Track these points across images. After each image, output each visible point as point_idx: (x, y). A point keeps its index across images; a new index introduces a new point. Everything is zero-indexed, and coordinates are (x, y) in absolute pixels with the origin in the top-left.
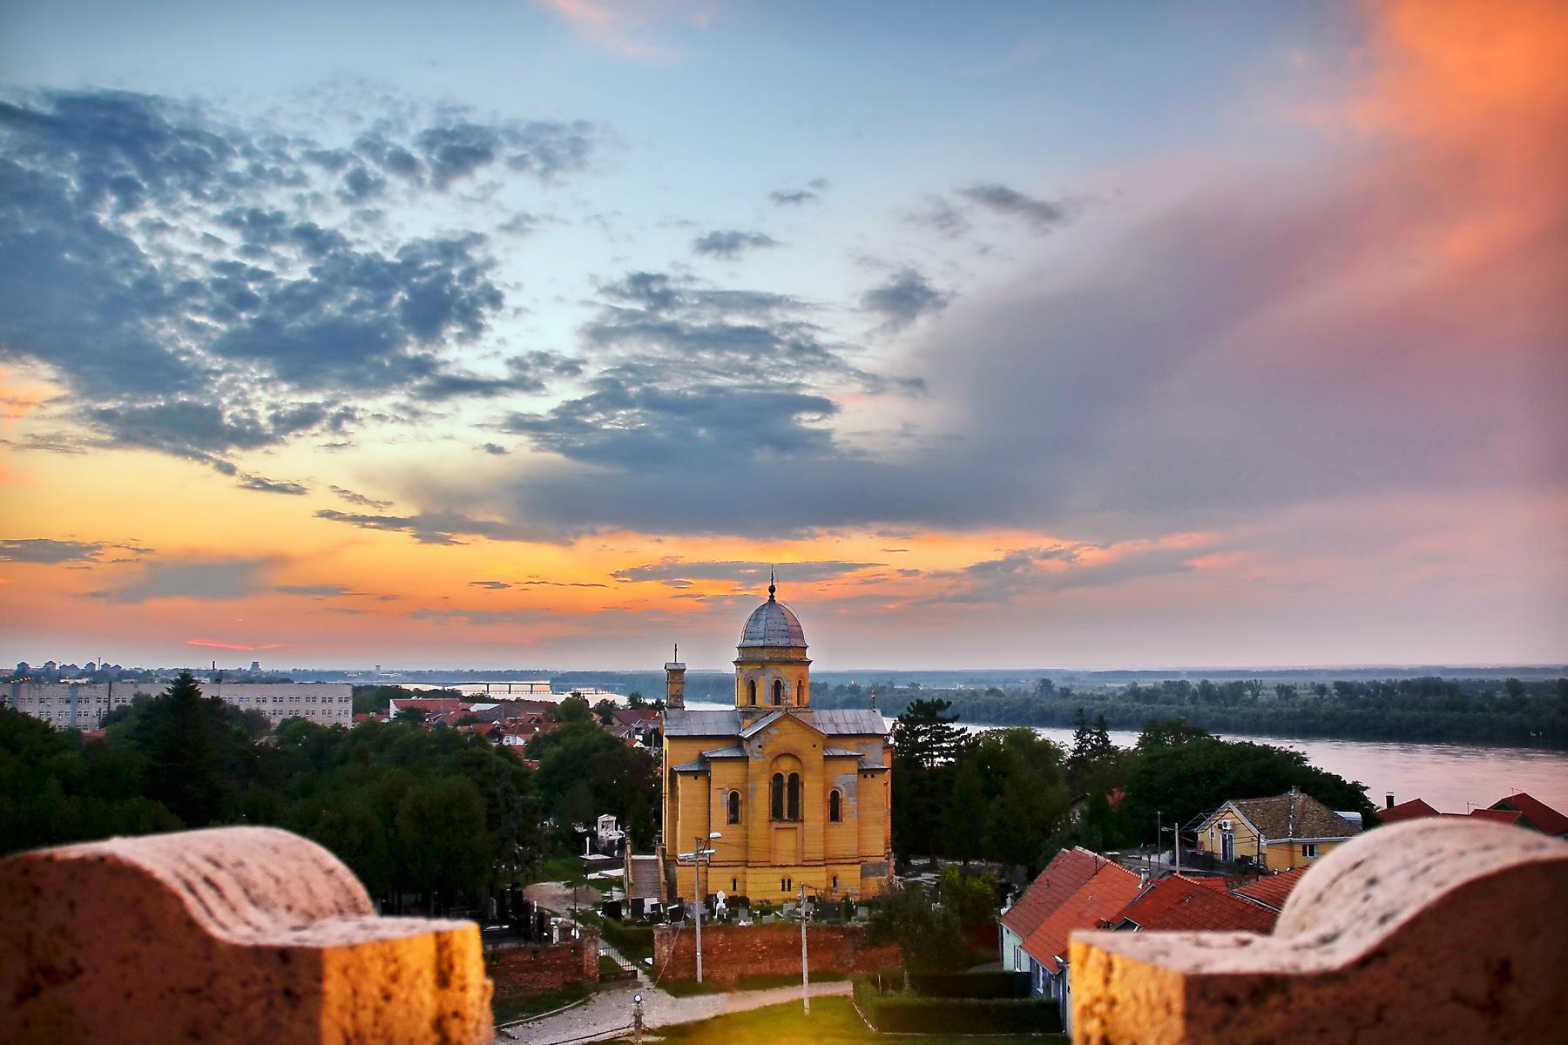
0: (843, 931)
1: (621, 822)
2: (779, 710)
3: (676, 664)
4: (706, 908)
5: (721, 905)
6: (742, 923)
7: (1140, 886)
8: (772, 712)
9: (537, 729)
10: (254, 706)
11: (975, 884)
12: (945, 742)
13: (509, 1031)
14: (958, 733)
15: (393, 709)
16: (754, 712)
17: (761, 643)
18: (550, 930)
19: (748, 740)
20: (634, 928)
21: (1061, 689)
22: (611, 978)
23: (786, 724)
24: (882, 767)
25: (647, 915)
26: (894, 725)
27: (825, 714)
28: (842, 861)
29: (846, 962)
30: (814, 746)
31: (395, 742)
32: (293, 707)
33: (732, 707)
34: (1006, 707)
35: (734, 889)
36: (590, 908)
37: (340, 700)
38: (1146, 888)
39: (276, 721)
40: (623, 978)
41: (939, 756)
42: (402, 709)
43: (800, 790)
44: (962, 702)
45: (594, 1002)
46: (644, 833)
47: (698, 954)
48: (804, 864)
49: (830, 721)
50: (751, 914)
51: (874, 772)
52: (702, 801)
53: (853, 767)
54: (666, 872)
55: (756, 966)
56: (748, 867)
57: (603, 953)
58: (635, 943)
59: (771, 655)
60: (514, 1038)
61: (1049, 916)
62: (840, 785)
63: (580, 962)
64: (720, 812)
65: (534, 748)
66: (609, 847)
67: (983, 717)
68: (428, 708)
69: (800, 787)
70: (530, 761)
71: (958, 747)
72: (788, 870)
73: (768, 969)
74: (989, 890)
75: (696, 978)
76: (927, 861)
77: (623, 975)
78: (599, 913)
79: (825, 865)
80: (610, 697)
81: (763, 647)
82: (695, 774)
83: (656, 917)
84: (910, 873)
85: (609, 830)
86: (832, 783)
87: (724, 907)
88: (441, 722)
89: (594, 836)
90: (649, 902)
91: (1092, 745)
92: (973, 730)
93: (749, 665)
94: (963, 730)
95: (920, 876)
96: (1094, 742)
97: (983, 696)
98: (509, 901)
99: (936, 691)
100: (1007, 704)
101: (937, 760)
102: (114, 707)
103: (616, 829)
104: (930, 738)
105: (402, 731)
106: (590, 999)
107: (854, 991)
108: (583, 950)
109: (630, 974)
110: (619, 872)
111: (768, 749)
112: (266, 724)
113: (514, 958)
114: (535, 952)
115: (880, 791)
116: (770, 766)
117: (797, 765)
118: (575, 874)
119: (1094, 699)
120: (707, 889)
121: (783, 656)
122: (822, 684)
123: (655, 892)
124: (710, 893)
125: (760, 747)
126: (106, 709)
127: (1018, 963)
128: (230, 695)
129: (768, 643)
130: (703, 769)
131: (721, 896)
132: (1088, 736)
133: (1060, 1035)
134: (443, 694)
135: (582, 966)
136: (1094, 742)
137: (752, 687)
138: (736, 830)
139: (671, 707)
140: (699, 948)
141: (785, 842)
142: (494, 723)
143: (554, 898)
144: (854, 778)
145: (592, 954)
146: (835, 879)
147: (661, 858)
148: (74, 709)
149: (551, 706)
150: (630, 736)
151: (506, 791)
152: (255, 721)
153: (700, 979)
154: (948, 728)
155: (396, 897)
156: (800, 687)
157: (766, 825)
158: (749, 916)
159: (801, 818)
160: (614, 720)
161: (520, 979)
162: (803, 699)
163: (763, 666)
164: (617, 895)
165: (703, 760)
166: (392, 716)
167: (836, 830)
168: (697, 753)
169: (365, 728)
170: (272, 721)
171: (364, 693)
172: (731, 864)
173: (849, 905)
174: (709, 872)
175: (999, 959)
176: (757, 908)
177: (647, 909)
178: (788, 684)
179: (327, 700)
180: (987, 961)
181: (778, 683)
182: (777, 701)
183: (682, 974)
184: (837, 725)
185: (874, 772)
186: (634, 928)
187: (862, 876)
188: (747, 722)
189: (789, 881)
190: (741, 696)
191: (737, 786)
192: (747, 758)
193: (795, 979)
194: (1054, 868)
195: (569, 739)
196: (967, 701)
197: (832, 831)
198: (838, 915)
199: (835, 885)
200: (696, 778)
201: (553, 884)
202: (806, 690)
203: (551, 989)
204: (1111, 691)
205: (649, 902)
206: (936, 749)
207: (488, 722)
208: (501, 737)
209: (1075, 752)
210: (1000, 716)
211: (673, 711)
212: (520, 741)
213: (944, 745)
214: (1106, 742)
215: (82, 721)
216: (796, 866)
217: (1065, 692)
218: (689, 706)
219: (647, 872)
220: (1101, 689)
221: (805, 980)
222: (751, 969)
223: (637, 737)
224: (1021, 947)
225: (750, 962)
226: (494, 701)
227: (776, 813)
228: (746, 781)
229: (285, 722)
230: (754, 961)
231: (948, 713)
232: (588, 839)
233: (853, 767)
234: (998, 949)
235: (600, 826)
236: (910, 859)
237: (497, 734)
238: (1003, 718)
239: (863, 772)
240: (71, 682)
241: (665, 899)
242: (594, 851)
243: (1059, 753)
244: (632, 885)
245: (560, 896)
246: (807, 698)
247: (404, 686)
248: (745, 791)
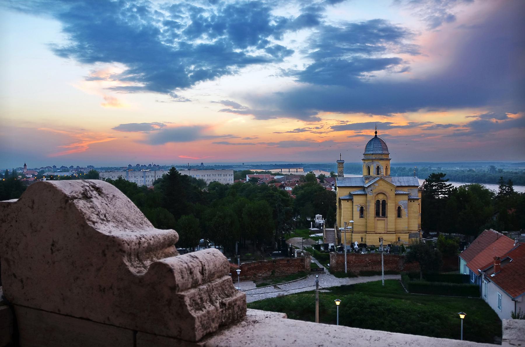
0: (399, 257)
1: (324, 217)
2: (378, 177)
3: (341, 160)
4: (351, 247)
5: (356, 246)
6: (363, 253)
7: (514, 245)
8: (376, 178)
9: (297, 184)
10: (201, 178)
11: (450, 242)
12: (443, 189)
13: (279, 286)
14: (448, 186)
15: (248, 178)
16: (369, 178)
17: (372, 153)
18: (294, 253)
19: (367, 188)
20: (324, 253)
21: (499, 169)
22: (315, 270)
23: (381, 182)
24: (417, 198)
25: (329, 249)
26: (424, 183)
27: (396, 178)
28: (402, 232)
29: (400, 268)
30: (392, 190)
31: (246, 189)
32: (214, 178)
33: (362, 176)
34: (476, 177)
35: (362, 241)
36: (310, 246)
37: (229, 175)
38: (517, 246)
39: (208, 183)
40: (319, 270)
41: (441, 194)
42: (250, 178)
43: (386, 206)
44: (458, 174)
45: (308, 278)
46: (331, 222)
47: (346, 263)
48: (388, 233)
49: (398, 181)
50: (367, 250)
51: (414, 200)
52: (350, 209)
53: (406, 198)
54: (338, 235)
55: (366, 268)
56: (367, 233)
57: (312, 261)
58: (324, 260)
59: (375, 157)
60: (280, 289)
61: (478, 254)
62: (401, 205)
63: (304, 264)
64: (357, 214)
65: (293, 192)
66: (320, 226)
67: (466, 180)
68: (260, 178)
69: (386, 205)
70: (294, 196)
71: (449, 191)
72: (382, 235)
73: (371, 269)
74: (456, 244)
75: (345, 271)
76: (436, 233)
77: (319, 269)
78: (313, 248)
79: (395, 233)
80: (323, 173)
81: (373, 154)
82: (347, 200)
83: (333, 250)
84: (429, 237)
85: (319, 220)
86: (398, 204)
87: (358, 247)
88: (263, 182)
89: (314, 222)
90: (331, 245)
91: (506, 191)
92: (456, 185)
93: (367, 160)
94: (450, 185)
95: (433, 238)
96: (507, 190)
97: (467, 172)
98: (281, 243)
99: (448, 170)
100: (476, 175)
101: (440, 196)
102: (157, 179)
103: (322, 220)
104: (438, 187)
105: (249, 185)
106: (307, 277)
107: (401, 278)
108: (305, 260)
109: (321, 269)
110: (321, 234)
111: (374, 191)
112: (205, 184)
113: (281, 262)
114: (288, 261)
115: (416, 207)
116: (375, 197)
117: (385, 197)
118: (306, 235)
119: (512, 174)
120: (352, 241)
121: (380, 157)
122: (404, 168)
123: (334, 241)
124: (353, 242)
125: (371, 190)
126: (154, 179)
127: (465, 271)
128: (197, 175)
129: (374, 152)
130: (350, 198)
131: (356, 243)
132: (504, 187)
133: (479, 298)
134: (266, 173)
135: (305, 266)
136: (507, 190)
137: (369, 169)
138: (362, 220)
139: (339, 176)
140: (346, 261)
141: (380, 225)
142: (282, 182)
143: (298, 243)
144: (406, 202)
145: (308, 262)
146: (399, 238)
147: (336, 230)
148: (145, 179)
149: (302, 177)
150: (330, 187)
151: (279, 206)
152: (201, 183)
153: (346, 272)
154: (445, 184)
155: (244, 241)
156: (386, 169)
157: (373, 218)
158: (366, 250)
159: (386, 216)
160: (325, 181)
161: (283, 269)
162: (388, 173)
163: (372, 161)
164: (320, 242)
165: (351, 195)
166: (247, 181)
167: (399, 220)
168: (349, 192)
169: (236, 184)
170: (207, 183)
171: (238, 173)
172: (361, 232)
173: (403, 248)
174: (346, 234)
175: (458, 269)
176: (369, 248)
177: (330, 247)
178: (382, 167)
179: (231, 175)
180: (455, 270)
181: (378, 167)
182: (378, 174)
183: (340, 270)
184: (400, 182)
185: (414, 200)
186: (324, 253)
187: (409, 238)
188: (367, 181)
190: (365, 172)
191: (363, 205)
192: (367, 194)
193: (379, 274)
194: (481, 237)
195: (305, 188)
196: (460, 174)
197: (398, 221)
198: (399, 251)
200: (348, 201)
201: (299, 238)
202: (389, 170)
203: (294, 273)
204: (521, 170)
205: (331, 245)
206: (440, 192)
207: (279, 182)
208: (284, 187)
209: (499, 193)
210: (473, 180)
211: (340, 177)
212: (291, 189)
213: (443, 190)
214: (512, 190)
215: (147, 183)
216: (385, 233)
217: (500, 171)
218: (345, 176)
219: (331, 234)
220: (516, 169)
221: (383, 274)
222: (365, 269)
223: (333, 187)
224: (466, 265)
225: (365, 267)
226: (283, 175)
227: (377, 214)
228: (366, 203)
229: (211, 183)
230: (366, 266)
231: (445, 178)
232: (312, 223)
233: (406, 198)
234: (458, 266)
235: (316, 218)
236: (429, 232)
237: (283, 186)
238: (474, 180)
239: (410, 200)
240: (144, 170)
241: (337, 244)
242: (314, 227)
243: (492, 194)
244: (325, 239)
245: (300, 242)
246: (389, 173)
247: (251, 170)
248: (366, 207)
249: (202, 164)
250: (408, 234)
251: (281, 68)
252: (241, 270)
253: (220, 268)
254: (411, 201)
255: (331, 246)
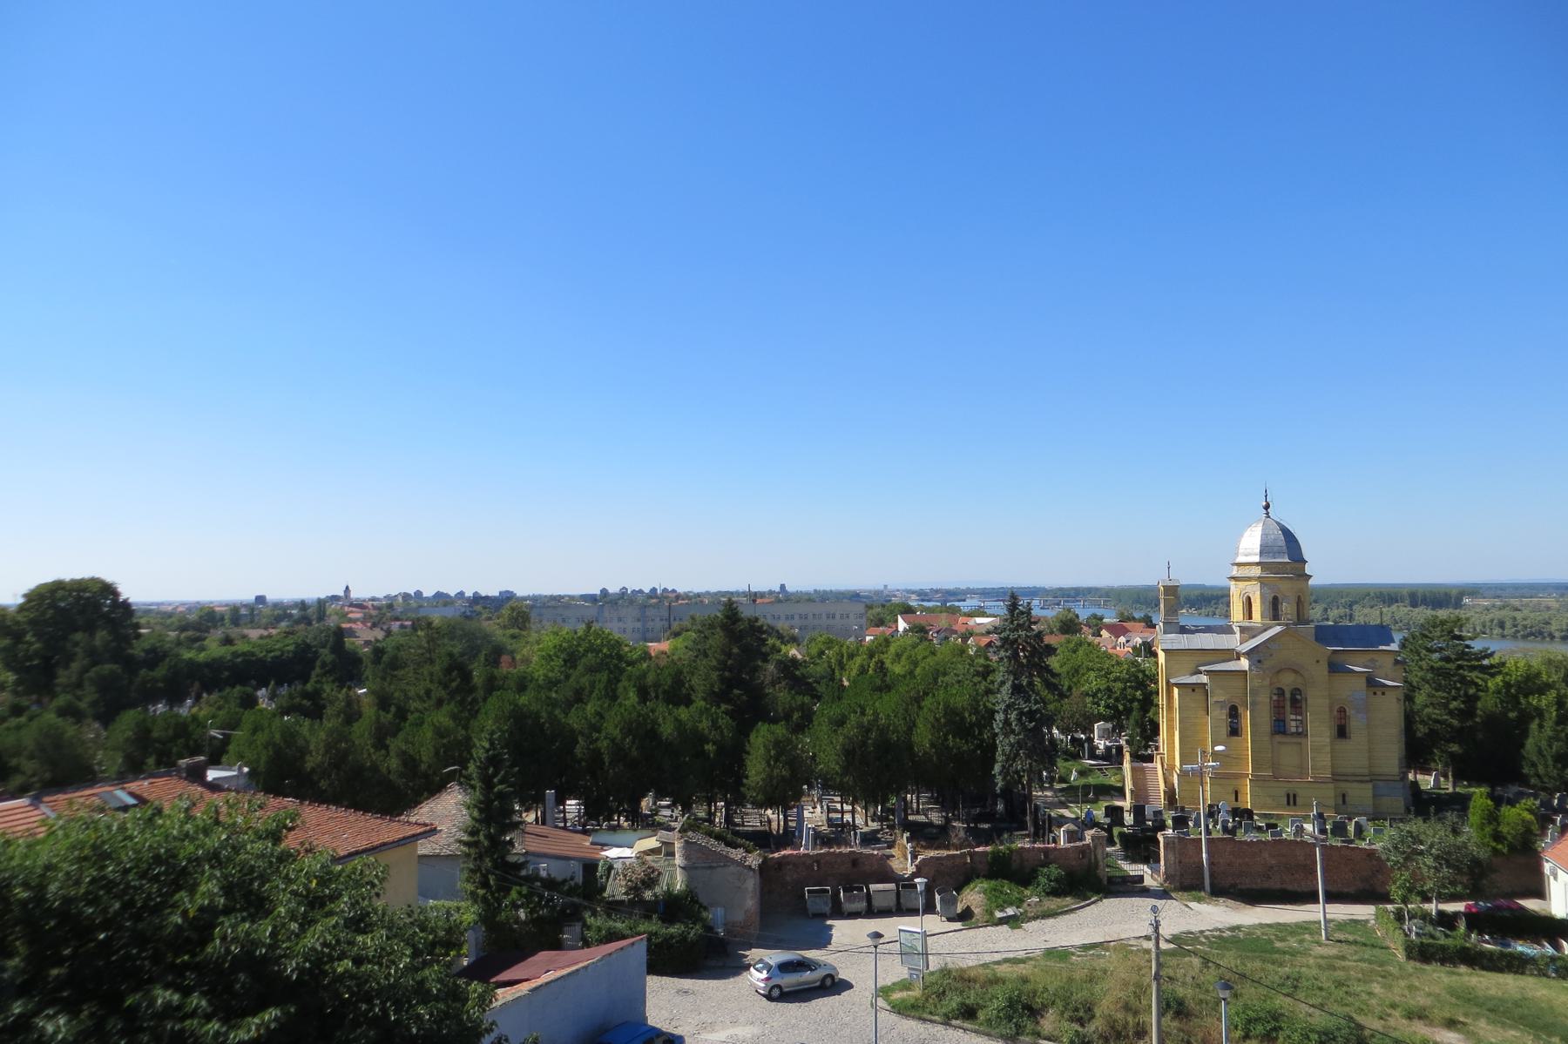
30: (1318, 662)
146: (1344, 796)
157: (1267, 738)
167: (1343, 745)
189: (1295, 796)
199: (1344, 802)
249: (783, 587)
250: (1370, 786)
251: (243, 717)
252: (926, 880)
253: (479, 641)
254: (1375, 693)
255: (1154, 812)
